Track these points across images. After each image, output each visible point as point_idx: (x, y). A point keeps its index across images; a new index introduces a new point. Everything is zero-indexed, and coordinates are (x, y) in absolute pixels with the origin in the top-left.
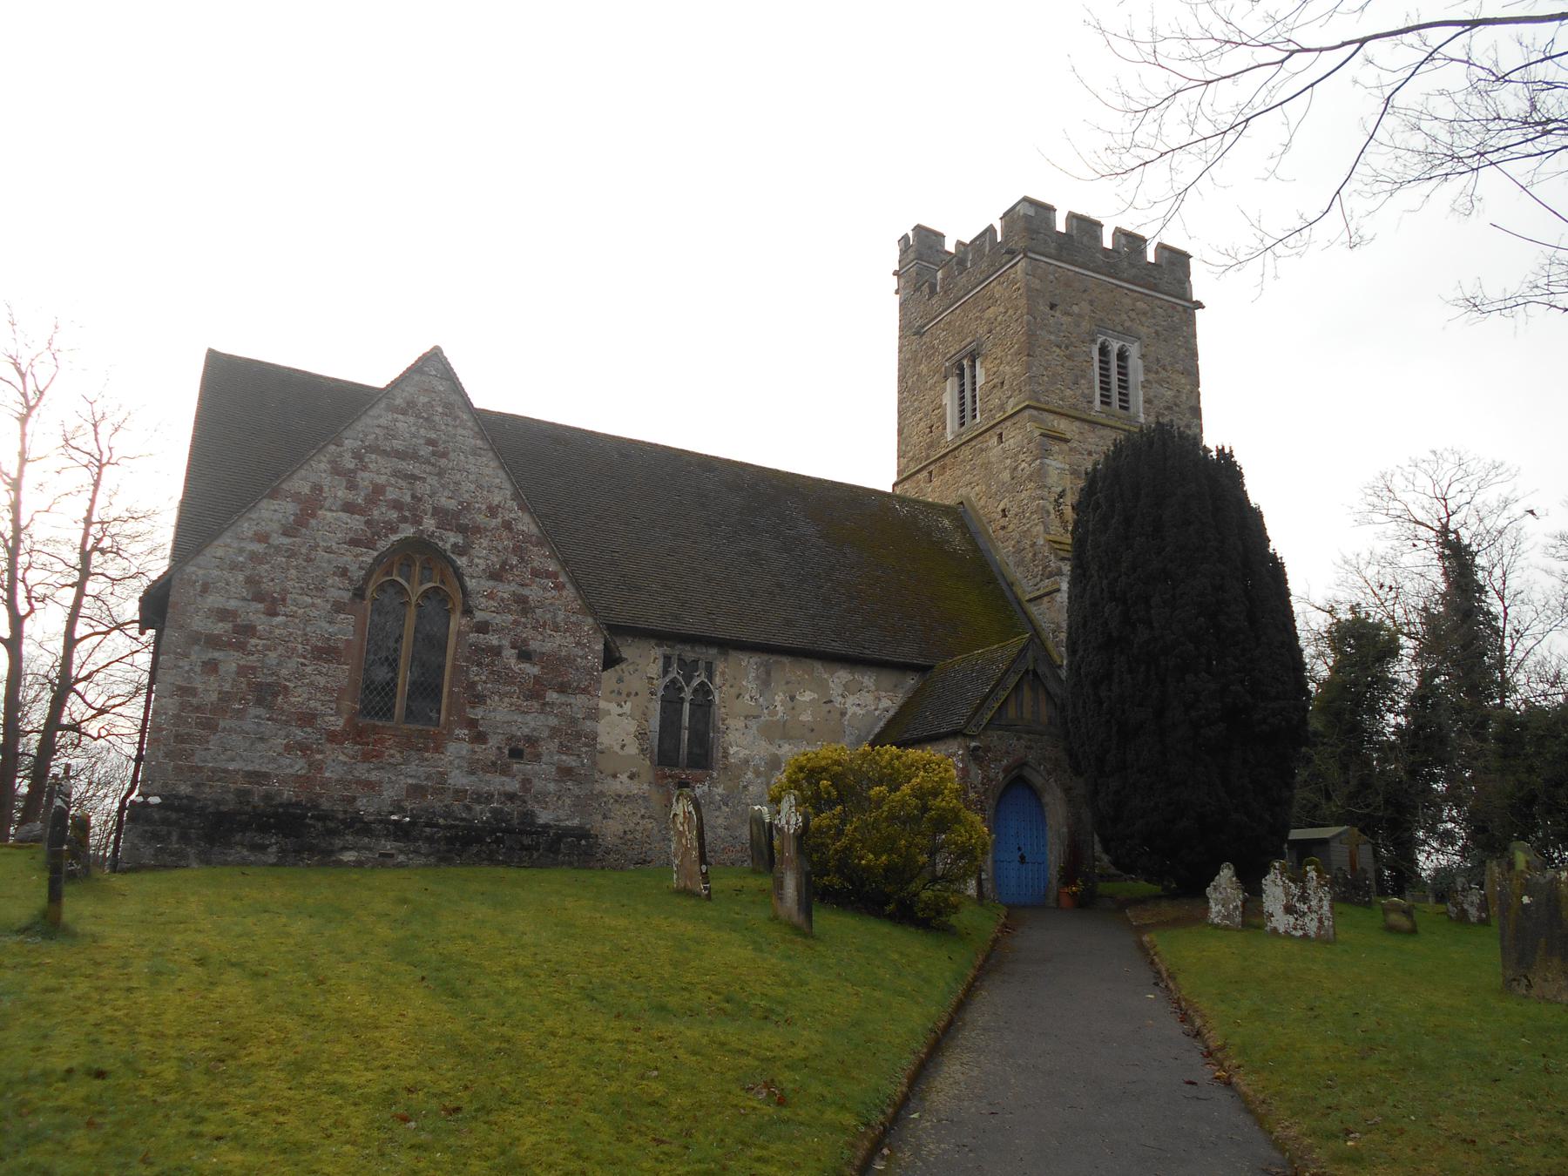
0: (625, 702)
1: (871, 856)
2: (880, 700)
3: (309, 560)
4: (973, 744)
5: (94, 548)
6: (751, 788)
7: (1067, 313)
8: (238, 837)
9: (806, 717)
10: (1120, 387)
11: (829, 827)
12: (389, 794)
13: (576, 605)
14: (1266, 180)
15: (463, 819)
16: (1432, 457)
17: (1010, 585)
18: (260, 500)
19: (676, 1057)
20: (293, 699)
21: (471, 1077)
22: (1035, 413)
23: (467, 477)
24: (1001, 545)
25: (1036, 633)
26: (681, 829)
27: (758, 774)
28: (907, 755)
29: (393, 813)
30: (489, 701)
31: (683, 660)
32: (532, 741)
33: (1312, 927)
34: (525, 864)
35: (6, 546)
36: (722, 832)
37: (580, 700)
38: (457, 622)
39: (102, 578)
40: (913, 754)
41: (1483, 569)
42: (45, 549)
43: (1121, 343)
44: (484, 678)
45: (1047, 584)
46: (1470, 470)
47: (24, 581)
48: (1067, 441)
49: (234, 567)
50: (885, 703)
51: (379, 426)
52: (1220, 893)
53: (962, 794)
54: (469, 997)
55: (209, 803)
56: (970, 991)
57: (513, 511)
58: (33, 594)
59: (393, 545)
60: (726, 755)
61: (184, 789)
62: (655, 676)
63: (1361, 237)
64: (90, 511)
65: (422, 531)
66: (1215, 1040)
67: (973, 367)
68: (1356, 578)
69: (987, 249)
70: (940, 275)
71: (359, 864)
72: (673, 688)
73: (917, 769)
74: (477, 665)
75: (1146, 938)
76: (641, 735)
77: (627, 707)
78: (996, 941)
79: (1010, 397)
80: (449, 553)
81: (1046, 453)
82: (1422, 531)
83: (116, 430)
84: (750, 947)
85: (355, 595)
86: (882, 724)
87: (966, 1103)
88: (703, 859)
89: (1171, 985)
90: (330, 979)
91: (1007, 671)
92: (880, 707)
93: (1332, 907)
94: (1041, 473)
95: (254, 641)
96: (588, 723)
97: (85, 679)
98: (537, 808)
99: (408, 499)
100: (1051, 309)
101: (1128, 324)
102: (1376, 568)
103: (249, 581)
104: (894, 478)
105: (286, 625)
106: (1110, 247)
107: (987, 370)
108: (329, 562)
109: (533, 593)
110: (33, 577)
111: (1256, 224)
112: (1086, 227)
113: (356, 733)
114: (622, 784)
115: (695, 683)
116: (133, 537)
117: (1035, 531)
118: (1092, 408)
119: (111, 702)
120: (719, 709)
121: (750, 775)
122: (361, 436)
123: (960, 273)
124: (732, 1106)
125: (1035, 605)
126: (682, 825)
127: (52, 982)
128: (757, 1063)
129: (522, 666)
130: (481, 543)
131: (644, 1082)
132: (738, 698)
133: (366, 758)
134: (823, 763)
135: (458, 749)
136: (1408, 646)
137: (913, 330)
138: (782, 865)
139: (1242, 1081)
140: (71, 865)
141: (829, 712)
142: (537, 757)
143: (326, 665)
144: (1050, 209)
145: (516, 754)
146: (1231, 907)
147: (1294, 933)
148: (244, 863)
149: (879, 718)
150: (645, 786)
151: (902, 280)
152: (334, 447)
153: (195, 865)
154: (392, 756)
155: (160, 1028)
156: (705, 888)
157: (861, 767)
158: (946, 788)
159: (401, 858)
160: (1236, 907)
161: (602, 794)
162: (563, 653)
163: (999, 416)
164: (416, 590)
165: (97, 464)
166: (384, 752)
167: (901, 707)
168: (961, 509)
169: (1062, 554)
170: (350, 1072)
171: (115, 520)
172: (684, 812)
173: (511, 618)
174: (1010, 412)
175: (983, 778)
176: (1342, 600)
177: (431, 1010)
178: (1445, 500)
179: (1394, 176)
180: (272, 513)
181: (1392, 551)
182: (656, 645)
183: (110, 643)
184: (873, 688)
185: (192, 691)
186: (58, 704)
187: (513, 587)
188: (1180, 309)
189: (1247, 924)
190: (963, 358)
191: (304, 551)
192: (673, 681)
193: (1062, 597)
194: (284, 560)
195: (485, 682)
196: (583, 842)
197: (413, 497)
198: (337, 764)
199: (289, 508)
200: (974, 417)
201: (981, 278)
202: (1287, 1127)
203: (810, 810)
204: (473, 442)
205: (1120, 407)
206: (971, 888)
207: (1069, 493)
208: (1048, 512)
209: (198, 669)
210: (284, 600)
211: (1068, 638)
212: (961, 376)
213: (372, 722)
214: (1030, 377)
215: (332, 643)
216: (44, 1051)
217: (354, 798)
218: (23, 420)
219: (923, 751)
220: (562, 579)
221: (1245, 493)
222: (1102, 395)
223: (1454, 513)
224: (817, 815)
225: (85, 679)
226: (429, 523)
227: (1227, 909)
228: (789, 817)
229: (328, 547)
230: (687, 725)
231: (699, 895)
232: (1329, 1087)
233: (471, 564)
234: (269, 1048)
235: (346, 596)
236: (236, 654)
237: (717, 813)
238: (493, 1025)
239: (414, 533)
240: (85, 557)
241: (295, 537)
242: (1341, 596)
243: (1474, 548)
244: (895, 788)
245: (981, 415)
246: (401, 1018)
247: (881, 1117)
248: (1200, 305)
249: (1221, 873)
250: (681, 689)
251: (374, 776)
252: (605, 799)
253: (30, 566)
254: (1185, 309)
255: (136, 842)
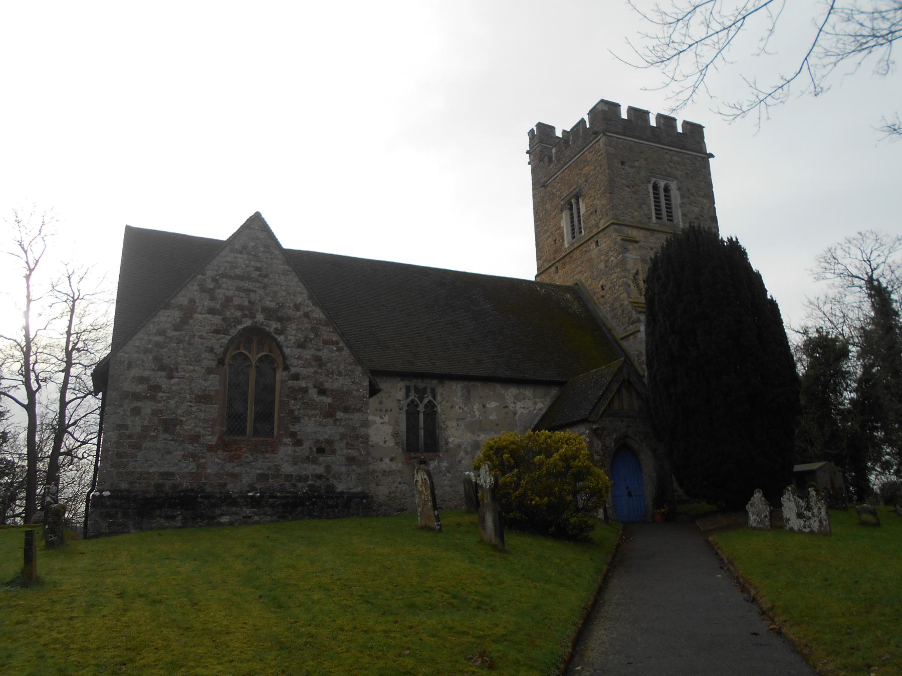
0: (385, 416)
1: (538, 499)
2: (536, 404)
3: (190, 344)
4: (594, 427)
5: (73, 349)
6: (463, 462)
7: (632, 167)
8: (158, 512)
9: (493, 417)
10: (667, 208)
11: (511, 483)
12: (246, 480)
13: (351, 360)
14: (758, 55)
15: (291, 492)
16: (859, 237)
17: (610, 330)
18: (159, 311)
19: (421, 639)
20: (186, 427)
21: (286, 664)
22: (617, 227)
23: (281, 288)
24: (602, 307)
25: (627, 357)
26: (421, 489)
27: (466, 452)
28: (555, 435)
29: (249, 492)
30: (302, 421)
31: (418, 388)
32: (330, 442)
33: (815, 526)
34: (331, 517)
35: (22, 350)
36: (447, 489)
37: (357, 416)
38: (280, 375)
39: (79, 366)
40: (559, 434)
41: (896, 301)
42: (45, 351)
43: (666, 182)
44: (298, 407)
45: (632, 328)
46: (883, 243)
47: (33, 370)
48: (637, 242)
49: (146, 351)
50: (540, 405)
51: (227, 262)
52: (755, 508)
53: (590, 457)
54: (289, 607)
55: (139, 493)
56: (606, 580)
57: (308, 306)
58: (40, 378)
59: (239, 332)
60: (447, 443)
61: (124, 486)
62: (401, 399)
63: (821, 88)
64: (70, 327)
65: (255, 322)
66: (766, 605)
67: (578, 203)
68: (818, 312)
69: (581, 133)
70: (554, 151)
71: (231, 524)
72: (412, 405)
73: (562, 443)
74: (294, 400)
75: (711, 539)
76: (396, 435)
77: (386, 418)
78: (618, 546)
79: (601, 219)
80: (273, 334)
81: (625, 250)
82: (856, 281)
83: (81, 279)
84: (467, 561)
85: (218, 363)
86: (538, 418)
87: (611, 657)
88: (435, 507)
89: (731, 568)
90: (201, 601)
91: (611, 382)
92: (537, 408)
93: (827, 513)
94: (623, 263)
95: (161, 394)
96: (363, 429)
97: (73, 424)
98: (335, 482)
99: (246, 303)
100: (622, 164)
101: (669, 170)
102: (829, 306)
103: (156, 359)
104: (536, 273)
105: (179, 384)
106: (655, 125)
107: (586, 204)
108: (202, 344)
109: (325, 354)
110: (38, 367)
111: (753, 86)
112: (638, 115)
113: (224, 445)
114: (386, 465)
115: (426, 401)
116: (96, 341)
117: (622, 296)
118: (651, 222)
119: (89, 437)
120: (441, 415)
121: (462, 454)
122: (216, 268)
123: (566, 149)
124: (459, 671)
125: (625, 341)
126: (421, 487)
127: (22, 617)
128: (473, 640)
129: (321, 398)
130: (292, 327)
131: (400, 659)
132: (452, 408)
133: (231, 459)
134: (504, 443)
135: (286, 451)
136: (853, 350)
137: (540, 185)
138: (483, 508)
139: (791, 632)
140: (51, 537)
141: (507, 413)
142: (334, 452)
143: (204, 406)
144: (617, 106)
145: (321, 451)
146: (763, 516)
147: (804, 530)
148: (163, 528)
149: (537, 415)
150: (400, 465)
151: (532, 156)
152: (200, 276)
153: (133, 531)
154: (247, 457)
155: (86, 644)
156: (438, 525)
157: (527, 444)
158: (580, 454)
159: (256, 518)
160: (766, 516)
161: (374, 471)
162: (345, 389)
163: (595, 231)
164: (254, 357)
165: (72, 300)
166: (242, 456)
167: (549, 407)
168: (576, 287)
169: (640, 309)
170: (207, 666)
171: (84, 331)
172: (422, 480)
173: (312, 370)
174: (602, 228)
175: (602, 447)
176: (810, 326)
177: (264, 618)
178: (869, 261)
179: (838, 51)
180: (166, 318)
181: (839, 295)
182: (401, 380)
183: (85, 403)
184: (532, 397)
185: (125, 427)
186: (58, 441)
187: (312, 352)
188: (700, 159)
189: (773, 527)
190: (571, 198)
191: (187, 338)
192: (413, 401)
193: (642, 335)
194: (175, 345)
195: (299, 409)
196: (365, 501)
197: (250, 302)
198: (214, 464)
199: (177, 314)
200: (581, 232)
201: (579, 150)
202: (826, 663)
203: (498, 473)
204: (283, 267)
205: (668, 220)
206: (601, 514)
207: (640, 272)
208: (629, 285)
209: (128, 413)
210: (177, 368)
211: (647, 360)
212: (571, 209)
213: (233, 438)
214: (612, 206)
215: (207, 392)
216: (7, 666)
217: (226, 484)
218: (28, 277)
219: (565, 432)
220: (341, 344)
221: (749, 264)
222: (656, 214)
223: (875, 269)
224: (503, 476)
225: (73, 424)
226: (260, 317)
227: (760, 517)
228: (486, 479)
229: (201, 336)
230: (422, 426)
231: (434, 529)
232: (848, 634)
233: (286, 339)
234: (155, 653)
235: (214, 364)
236: (151, 403)
237: (444, 478)
238: (303, 625)
239: (251, 323)
240: (69, 354)
241: (182, 331)
242: (810, 323)
243: (890, 289)
244: (548, 456)
245: (585, 231)
246: (244, 626)
247: (557, 672)
248: (711, 156)
249: (755, 495)
250: (417, 406)
251: (237, 470)
252: (376, 474)
253: (36, 362)
254: (703, 158)
255: (97, 519)
